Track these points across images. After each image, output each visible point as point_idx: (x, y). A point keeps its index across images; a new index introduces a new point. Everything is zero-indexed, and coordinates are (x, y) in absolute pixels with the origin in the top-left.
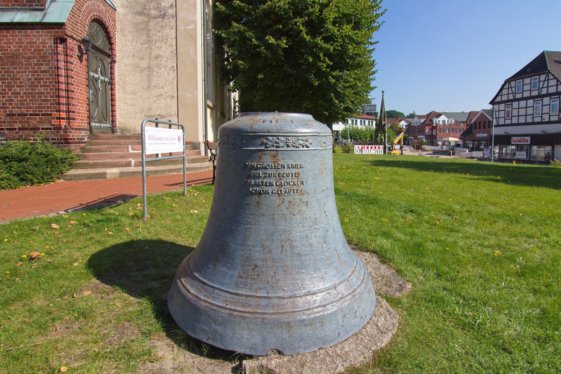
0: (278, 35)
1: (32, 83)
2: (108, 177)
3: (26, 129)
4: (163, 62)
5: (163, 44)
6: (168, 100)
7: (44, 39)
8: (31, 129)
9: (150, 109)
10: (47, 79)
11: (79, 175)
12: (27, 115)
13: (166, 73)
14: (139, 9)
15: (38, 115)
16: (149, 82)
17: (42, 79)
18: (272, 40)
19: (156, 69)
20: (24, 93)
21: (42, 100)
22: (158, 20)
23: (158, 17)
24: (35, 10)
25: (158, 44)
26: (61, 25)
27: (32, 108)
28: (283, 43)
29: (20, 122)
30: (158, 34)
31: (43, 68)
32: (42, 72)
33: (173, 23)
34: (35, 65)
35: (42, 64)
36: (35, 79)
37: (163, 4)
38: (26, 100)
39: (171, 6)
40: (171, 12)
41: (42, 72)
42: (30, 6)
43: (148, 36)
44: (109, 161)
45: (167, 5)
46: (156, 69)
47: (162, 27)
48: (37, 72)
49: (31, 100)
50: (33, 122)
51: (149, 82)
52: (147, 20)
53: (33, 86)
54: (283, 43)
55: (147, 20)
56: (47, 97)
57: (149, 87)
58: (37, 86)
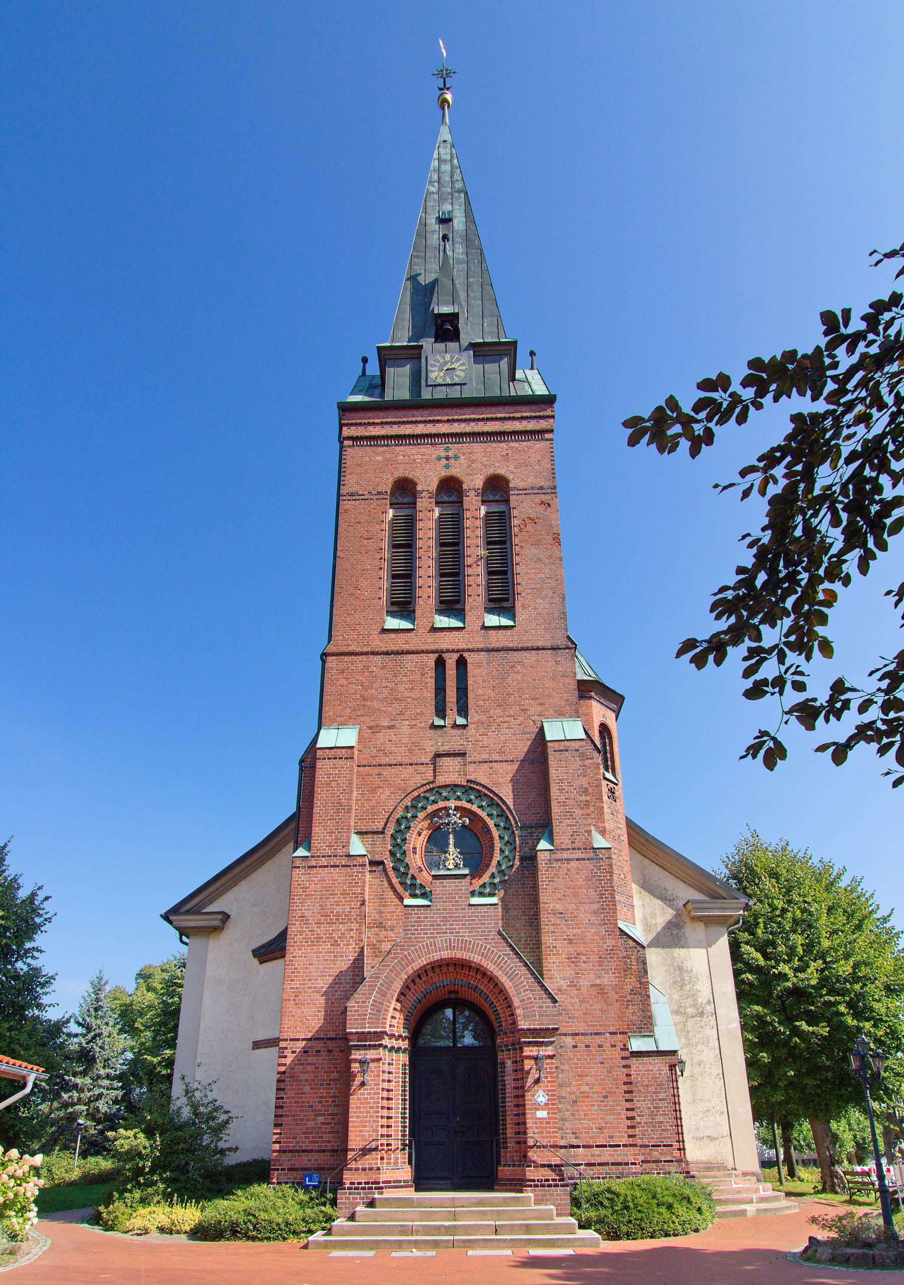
0: (812, 1019)
1: (652, 1112)
2: (749, 1214)
3: (649, 1162)
4: (707, 1069)
5: (704, 1047)
6: (717, 1116)
7: (659, 1066)
8: (653, 1162)
9: (698, 1129)
10: (666, 1107)
11: (539, 1240)
12: (648, 1146)
13: (711, 1083)
14: (675, 1007)
15: (660, 1146)
16: (694, 1094)
17: (660, 1107)
18: (804, 1026)
19: (699, 1078)
20: (645, 1123)
21: (663, 1130)
22: (696, 1019)
23: (696, 1016)
24: (644, 1036)
25: (699, 1048)
26: (674, 1053)
27: (653, 1138)
28: (823, 1030)
29: (643, 1154)
30: (698, 1036)
31: (662, 1096)
32: (661, 1100)
33: (713, 1022)
34: (654, 1093)
35: (660, 1092)
36: (655, 1108)
37: (700, 1000)
38: (647, 1130)
39: (708, 1002)
40: (709, 1008)
41: (661, 1100)
42: (640, 1032)
43: (687, 1038)
44: (729, 1196)
45: (705, 1001)
46: (699, 1078)
47: (701, 1027)
48: (654, 1100)
49: (652, 1131)
50: (655, 1154)
51: (694, 1094)
52: (684, 1019)
53: (652, 1115)
54: (823, 1030)
55: (684, 1019)
56: (332, 1102)
57: (694, 1101)
58: (657, 1115)
